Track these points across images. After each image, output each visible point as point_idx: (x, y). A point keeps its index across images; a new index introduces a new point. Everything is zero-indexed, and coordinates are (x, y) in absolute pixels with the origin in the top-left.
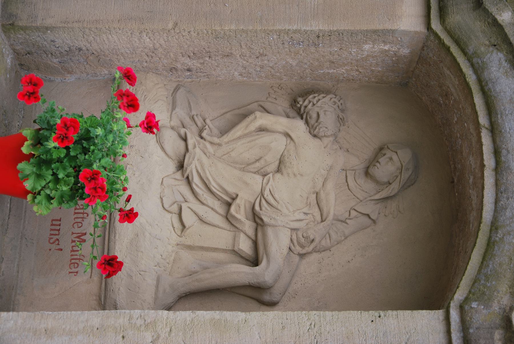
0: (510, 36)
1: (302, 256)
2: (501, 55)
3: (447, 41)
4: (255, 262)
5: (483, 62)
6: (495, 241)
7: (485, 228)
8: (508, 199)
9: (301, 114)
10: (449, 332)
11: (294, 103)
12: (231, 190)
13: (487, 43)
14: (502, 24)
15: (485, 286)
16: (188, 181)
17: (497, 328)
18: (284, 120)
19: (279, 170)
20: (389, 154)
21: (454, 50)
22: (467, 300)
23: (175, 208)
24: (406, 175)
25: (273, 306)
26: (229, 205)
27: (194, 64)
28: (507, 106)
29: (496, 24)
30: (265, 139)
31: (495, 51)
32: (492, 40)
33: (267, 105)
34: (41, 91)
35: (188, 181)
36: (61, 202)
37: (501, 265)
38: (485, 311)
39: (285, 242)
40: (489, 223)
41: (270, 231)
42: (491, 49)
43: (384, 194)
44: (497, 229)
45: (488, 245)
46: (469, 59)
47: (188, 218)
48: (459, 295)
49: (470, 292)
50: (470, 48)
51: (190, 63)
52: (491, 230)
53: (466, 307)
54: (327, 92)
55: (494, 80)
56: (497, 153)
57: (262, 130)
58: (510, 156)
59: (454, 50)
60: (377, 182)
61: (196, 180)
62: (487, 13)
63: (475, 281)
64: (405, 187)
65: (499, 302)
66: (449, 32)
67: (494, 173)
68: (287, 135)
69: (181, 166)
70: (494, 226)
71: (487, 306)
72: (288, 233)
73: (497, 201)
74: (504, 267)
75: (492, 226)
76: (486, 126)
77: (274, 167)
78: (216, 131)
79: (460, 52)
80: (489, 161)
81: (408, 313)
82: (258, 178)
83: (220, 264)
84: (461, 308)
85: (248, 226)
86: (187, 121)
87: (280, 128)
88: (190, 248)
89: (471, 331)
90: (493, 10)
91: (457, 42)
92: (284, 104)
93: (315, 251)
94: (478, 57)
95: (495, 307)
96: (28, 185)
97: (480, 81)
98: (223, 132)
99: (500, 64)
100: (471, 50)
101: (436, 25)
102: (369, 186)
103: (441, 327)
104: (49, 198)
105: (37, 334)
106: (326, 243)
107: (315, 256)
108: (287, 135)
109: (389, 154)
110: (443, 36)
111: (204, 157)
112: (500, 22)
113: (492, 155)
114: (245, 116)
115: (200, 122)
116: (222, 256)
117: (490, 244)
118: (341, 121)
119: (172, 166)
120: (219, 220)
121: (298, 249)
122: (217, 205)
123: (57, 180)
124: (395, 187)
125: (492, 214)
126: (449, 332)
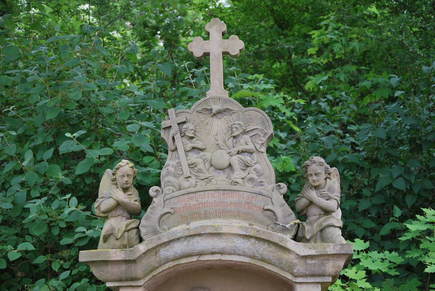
0: (153, 246)
2: (162, 250)
3: (150, 276)
5: (164, 259)
6: (261, 258)
7: (253, 262)
8: (239, 250)
10: (307, 283)
13: (154, 257)
14: (146, 250)
15: (285, 265)
17: (306, 262)
22: (292, 274)
25: (110, 289)
28: (189, 248)
29: (145, 253)
31: (159, 253)
32: (153, 254)
37: (274, 257)
38: (298, 267)
40: (251, 259)
42: (158, 255)
44: (255, 256)
45: (263, 261)
46: (161, 265)
48: (290, 277)
49: (287, 272)
50: (156, 265)
52: (255, 259)
53: (296, 274)
55: (175, 254)
56: (213, 253)
58: (216, 248)
62: (140, 257)
63: (282, 268)
65: (293, 259)
66: (146, 275)
67: (224, 255)
71: (296, 265)
73: (239, 255)
74: (275, 255)
75: (253, 258)
76: (198, 257)
79: (156, 270)
84: (296, 276)
89: (307, 273)
90: (138, 254)
91: (151, 271)
94: (161, 261)
95: (296, 261)
97: (173, 260)
99: (166, 250)
100: (156, 265)
101: (141, 283)
103: (305, 286)
112: (145, 251)
113: (214, 255)
117: (263, 260)
125: (246, 258)
126: (307, 283)
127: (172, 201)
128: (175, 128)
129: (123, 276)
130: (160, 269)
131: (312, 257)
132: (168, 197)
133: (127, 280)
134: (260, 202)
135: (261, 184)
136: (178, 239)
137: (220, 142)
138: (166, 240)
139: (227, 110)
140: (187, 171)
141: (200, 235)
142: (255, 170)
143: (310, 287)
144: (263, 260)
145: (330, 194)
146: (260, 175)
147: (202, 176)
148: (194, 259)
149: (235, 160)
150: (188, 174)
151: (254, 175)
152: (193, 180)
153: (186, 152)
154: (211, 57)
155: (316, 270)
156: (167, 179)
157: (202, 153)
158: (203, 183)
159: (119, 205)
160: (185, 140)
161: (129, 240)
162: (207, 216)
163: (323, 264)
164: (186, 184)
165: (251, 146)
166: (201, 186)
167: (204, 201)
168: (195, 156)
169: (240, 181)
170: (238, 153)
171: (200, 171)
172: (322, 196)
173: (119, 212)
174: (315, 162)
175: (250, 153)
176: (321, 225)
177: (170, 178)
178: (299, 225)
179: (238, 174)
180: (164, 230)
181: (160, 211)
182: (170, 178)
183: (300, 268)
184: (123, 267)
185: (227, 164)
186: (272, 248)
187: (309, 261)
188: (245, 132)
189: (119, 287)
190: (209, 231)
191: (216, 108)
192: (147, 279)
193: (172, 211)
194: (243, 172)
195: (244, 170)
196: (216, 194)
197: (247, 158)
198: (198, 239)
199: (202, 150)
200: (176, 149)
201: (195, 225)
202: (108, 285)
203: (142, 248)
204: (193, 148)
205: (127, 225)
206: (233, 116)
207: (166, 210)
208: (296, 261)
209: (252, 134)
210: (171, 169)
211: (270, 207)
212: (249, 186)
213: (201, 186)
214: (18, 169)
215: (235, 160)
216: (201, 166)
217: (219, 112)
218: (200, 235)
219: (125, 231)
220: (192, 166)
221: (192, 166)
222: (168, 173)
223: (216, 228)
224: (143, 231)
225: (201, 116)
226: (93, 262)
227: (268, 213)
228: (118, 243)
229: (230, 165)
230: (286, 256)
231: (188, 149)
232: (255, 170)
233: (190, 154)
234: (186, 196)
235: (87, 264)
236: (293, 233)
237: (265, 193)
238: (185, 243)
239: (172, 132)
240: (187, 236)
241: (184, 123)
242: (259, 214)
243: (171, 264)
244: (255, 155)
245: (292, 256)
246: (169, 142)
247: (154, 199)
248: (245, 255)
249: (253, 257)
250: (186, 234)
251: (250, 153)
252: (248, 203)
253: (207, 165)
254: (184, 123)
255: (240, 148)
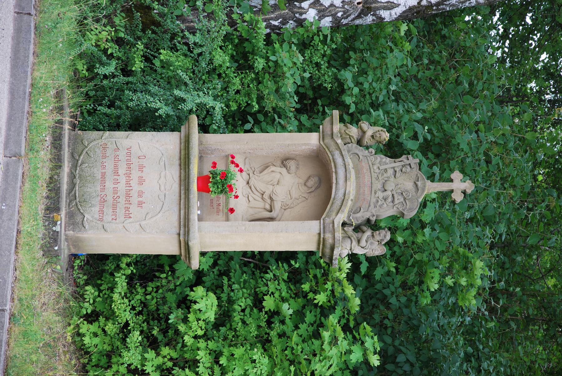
1: (285, 209)
3: (325, 147)
4: (271, 211)
9: (285, 166)
11: (282, 163)
12: (264, 190)
16: (250, 187)
18: (279, 168)
19: (278, 184)
20: (311, 178)
21: (326, 149)
23: (247, 196)
24: (316, 185)
26: (263, 195)
27: (252, 151)
29: (336, 143)
30: (274, 174)
33: (274, 163)
34: (217, 166)
35: (250, 187)
36: (218, 194)
39: (280, 205)
41: (275, 202)
43: (310, 191)
47: (250, 198)
48: (323, 217)
51: (250, 151)
54: (293, 159)
56: (336, 179)
57: (272, 171)
59: (326, 149)
60: (308, 187)
61: (253, 187)
64: (316, 189)
68: (281, 173)
69: (248, 183)
70: (334, 199)
72: (280, 203)
77: (276, 183)
78: (258, 172)
80: (334, 181)
81: (310, 221)
82: (272, 186)
83: (260, 212)
85: (269, 201)
86: (249, 169)
87: (278, 171)
88: (251, 207)
90: (336, 139)
91: (327, 147)
92: (279, 163)
93: (289, 208)
95: (331, 218)
96: (211, 189)
97: (333, 159)
98: (261, 172)
100: (331, 150)
101: (322, 143)
102: (306, 188)
103: (319, 224)
104: (215, 193)
105: (72, 326)
106: (292, 206)
107: (289, 210)
108: (281, 173)
109: (311, 178)
110: (324, 145)
111: (255, 181)
114: (267, 167)
115: (253, 169)
116: (260, 210)
117: (333, 203)
118: (297, 168)
119: (245, 183)
120: (260, 200)
121: (284, 208)
122: (259, 195)
123: (218, 187)
124: (313, 189)
127: (366, 160)
128: (408, 162)
129: (325, 133)
130: (328, 152)
131: (333, 226)
132: (368, 158)
133: (323, 135)
134: (365, 205)
135: (375, 207)
136: (344, 160)
137: (399, 186)
138: (343, 153)
139: (418, 189)
140: (382, 167)
141: (346, 171)
142: (383, 204)
143: (318, 227)
144: (333, 203)
145: (369, 242)
146: (381, 206)
147: (380, 176)
148: (334, 170)
149: (389, 193)
150: (381, 168)
151: (380, 203)
152: (377, 171)
153: (394, 168)
154: (451, 183)
155: (327, 229)
156: (379, 158)
157: (393, 176)
158: (376, 176)
159: (364, 132)
160: (401, 167)
161: (345, 138)
162: (357, 178)
163: (330, 232)
164: (375, 167)
165: (396, 202)
166: (374, 175)
167: (366, 177)
168: (391, 173)
169: (377, 195)
170: (393, 195)
171: (383, 175)
172: (368, 238)
173: (361, 134)
174: (386, 233)
175: (393, 201)
176: (352, 236)
177: (379, 159)
178: (352, 225)
179: (381, 195)
180: (350, 156)
181: (360, 154)
182: (379, 159)
183: (328, 221)
184: (329, 133)
185: (386, 188)
186: (338, 208)
187: (331, 225)
188: (405, 199)
189: (319, 132)
190: (348, 175)
191: (419, 183)
192: (324, 145)
193: (360, 160)
194: (382, 197)
195: (383, 198)
196: (369, 183)
197: (390, 199)
198: (344, 170)
199: (395, 177)
200: (395, 162)
201: (351, 165)
202: (321, 126)
203: (339, 141)
204: (396, 171)
205: (353, 137)
206: (415, 193)
207: (361, 157)
208: (331, 218)
209: (404, 203)
210: (384, 160)
211: (362, 210)
212: (374, 200)
213: (374, 175)
214: (392, 82)
215: (389, 193)
216: (385, 175)
217: (417, 185)
218: (346, 171)
219: (349, 135)
220: (386, 170)
221: (386, 170)
222: (381, 158)
223: (349, 179)
224: (350, 145)
225: (415, 176)
226: (332, 117)
227: (359, 209)
228: (343, 131)
229: (386, 190)
230: (334, 214)
231: (395, 169)
232: (383, 204)
233: (392, 170)
234: (368, 167)
235: (332, 115)
236: (348, 222)
237: (370, 208)
238: (342, 164)
239: (405, 160)
240: (345, 164)
241: (411, 167)
242: (358, 205)
243: (331, 158)
244: (392, 204)
245: (334, 217)
246: (400, 159)
247: (367, 151)
248: (335, 195)
249: (334, 199)
250: (347, 164)
251: (393, 201)
252: (364, 199)
253: (386, 179)
254: (411, 167)
255: (396, 196)
